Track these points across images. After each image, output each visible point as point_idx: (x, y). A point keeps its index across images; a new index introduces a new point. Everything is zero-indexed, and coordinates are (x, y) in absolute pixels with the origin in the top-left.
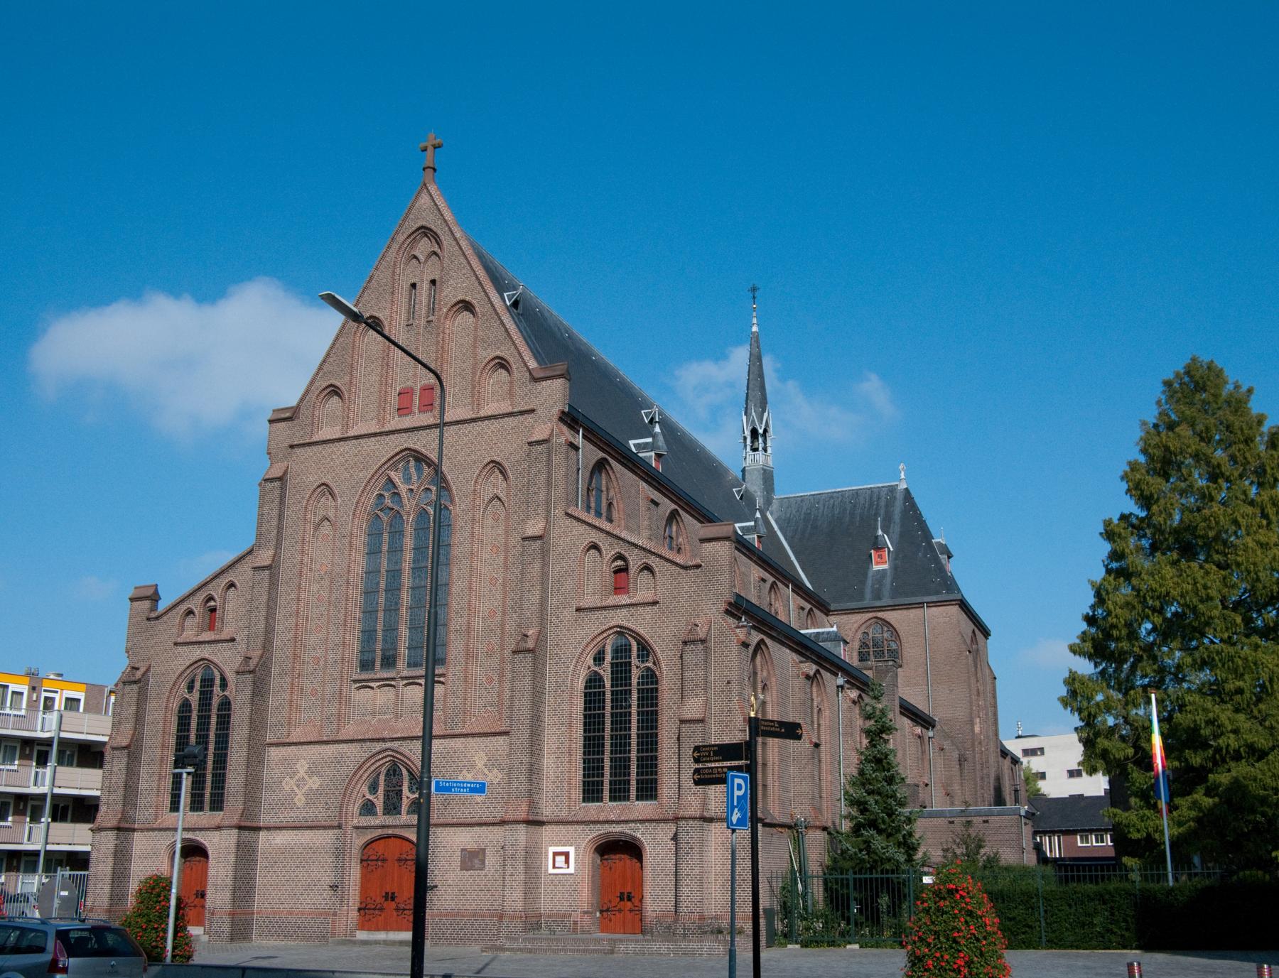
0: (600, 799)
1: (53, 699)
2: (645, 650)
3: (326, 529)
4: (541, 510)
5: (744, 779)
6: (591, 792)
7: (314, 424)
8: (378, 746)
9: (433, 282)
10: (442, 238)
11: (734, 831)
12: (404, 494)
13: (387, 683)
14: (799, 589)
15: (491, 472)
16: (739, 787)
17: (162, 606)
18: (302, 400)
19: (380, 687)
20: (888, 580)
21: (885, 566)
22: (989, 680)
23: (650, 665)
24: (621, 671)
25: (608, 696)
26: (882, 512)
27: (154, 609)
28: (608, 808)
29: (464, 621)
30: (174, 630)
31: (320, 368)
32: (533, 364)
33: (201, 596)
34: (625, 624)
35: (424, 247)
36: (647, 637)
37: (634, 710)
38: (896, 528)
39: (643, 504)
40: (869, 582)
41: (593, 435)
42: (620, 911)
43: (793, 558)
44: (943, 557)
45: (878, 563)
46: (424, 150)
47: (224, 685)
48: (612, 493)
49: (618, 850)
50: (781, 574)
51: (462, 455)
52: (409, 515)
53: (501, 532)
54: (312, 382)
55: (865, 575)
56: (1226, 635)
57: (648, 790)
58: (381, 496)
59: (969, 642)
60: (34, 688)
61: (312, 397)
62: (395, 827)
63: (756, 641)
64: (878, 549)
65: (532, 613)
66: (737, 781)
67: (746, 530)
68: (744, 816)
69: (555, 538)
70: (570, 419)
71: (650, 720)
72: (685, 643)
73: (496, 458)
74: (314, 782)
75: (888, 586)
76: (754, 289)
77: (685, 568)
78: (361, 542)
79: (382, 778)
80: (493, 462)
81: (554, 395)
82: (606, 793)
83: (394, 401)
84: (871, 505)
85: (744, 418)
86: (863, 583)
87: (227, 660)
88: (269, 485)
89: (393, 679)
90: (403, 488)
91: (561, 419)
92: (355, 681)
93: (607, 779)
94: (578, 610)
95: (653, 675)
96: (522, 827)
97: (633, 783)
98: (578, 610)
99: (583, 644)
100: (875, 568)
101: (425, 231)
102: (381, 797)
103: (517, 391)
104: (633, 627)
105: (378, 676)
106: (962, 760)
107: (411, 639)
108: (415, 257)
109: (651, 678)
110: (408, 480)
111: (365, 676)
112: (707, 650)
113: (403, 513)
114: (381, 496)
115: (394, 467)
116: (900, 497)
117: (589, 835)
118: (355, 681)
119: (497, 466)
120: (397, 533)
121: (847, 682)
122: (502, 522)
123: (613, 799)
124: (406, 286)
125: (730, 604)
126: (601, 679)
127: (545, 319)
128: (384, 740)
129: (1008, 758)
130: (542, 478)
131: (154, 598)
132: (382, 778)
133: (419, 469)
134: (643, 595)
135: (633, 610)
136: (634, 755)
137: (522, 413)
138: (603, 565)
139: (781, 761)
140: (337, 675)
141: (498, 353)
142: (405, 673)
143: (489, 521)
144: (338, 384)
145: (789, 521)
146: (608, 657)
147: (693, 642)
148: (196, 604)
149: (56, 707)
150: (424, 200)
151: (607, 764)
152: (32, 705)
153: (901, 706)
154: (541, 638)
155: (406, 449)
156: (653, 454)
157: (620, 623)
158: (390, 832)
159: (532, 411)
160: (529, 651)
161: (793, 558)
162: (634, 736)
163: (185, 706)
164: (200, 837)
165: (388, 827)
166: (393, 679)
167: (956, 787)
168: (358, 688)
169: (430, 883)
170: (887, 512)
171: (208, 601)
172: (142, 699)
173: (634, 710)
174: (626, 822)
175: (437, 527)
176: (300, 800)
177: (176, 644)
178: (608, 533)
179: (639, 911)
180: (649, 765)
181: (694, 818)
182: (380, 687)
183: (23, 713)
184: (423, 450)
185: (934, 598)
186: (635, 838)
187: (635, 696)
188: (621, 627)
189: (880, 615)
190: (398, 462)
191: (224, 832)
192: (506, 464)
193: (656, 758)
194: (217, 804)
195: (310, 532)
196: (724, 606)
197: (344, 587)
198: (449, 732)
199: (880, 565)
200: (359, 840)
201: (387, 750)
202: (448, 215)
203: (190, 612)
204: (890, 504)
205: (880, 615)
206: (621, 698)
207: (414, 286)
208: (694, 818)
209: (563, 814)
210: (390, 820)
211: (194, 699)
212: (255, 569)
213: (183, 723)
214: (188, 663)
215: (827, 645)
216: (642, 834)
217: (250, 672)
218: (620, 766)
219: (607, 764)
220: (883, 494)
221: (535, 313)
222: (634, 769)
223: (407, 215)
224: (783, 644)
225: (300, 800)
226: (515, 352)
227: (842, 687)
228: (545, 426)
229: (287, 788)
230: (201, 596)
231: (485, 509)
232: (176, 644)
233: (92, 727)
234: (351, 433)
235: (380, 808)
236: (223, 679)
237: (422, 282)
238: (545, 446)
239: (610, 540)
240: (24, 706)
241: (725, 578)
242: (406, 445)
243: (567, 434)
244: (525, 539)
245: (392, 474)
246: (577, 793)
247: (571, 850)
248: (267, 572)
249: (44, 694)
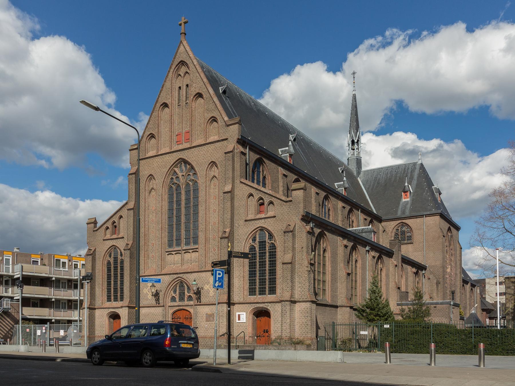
0: (255, 295)
1: (77, 265)
2: (271, 236)
3: (153, 193)
4: (230, 181)
6: (252, 292)
7: (146, 151)
8: (176, 276)
9: (187, 85)
10: (189, 65)
11: (217, 289)
12: (181, 177)
13: (178, 252)
15: (212, 166)
16: (219, 274)
17: (98, 225)
19: (176, 254)
20: (409, 206)
21: (408, 199)
22: (458, 249)
23: (273, 242)
24: (262, 244)
25: (258, 255)
26: (409, 175)
27: (95, 227)
28: (258, 298)
29: (204, 226)
30: (103, 235)
32: (226, 119)
33: (111, 221)
34: (264, 226)
35: (183, 69)
36: (271, 231)
37: (267, 260)
38: (415, 182)
39: (280, 176)
40: (400, 207)
41: (254, 148)
42: (264, 336)
43: (368, 197)
44: (437, 195)
45: (405, 198)
46: (180, 25)
47: (121, 255)
48: (265, 173)
49: (262, 314)
51: (198, 158)
52: (183, 184)
53: (217, 190)
55: (399, 204)
57: (273, 291)
58: (172, 178)
59: (445, 232)
60: (70, 261)
61: (144, 139)
62: (183, 306)
64: (405, 192)
65: (228, 223)
67: (339, 186)
69: (237, 192)
70: (242, 142)
71: (273, 263)
72: (285, 232)
73: (213, 160)
75: (408, 209)
76: (354, 73)
77: (286, 202)
78: (166, 197)
79: (178, 288)
80: (212, 162)
81: (234, 132)
82: (257, 292)
83: (175, 138)
84: (404, 172)
85: (349, 135)
86: (398, 207)
87: (121, 244)
88: (131, 176)
89: (180, 251)
90: (180, 174)
91: (238, 142)
92: (167, 252)
93: (257, 287)
94: (246, 221)
97: (267, 288)
98: (246, 221)
99: (248, 234)
100: (404, 200)
101: (183, 63)
102: (178, 295)
103: (221, 131)
104: (266, 227)
105: (175, 250)
106: (438, 283)
107: (186, 235)
108: (180, 75)
109: (273, 247)
110: (182, 171)
111: (170, 250)
112: (294, 236)
113: (180, 184)
114: (172, 178)
115: (176, 166)
117: (251, 307)
118: (167, 252)
119: (213, 164)
120: (179, 194)
122: (217, 187)
124: (177, 89)
125: (303, 216)
126: (255, 248)
127: (242, 97)
128: (177, 274)
129: (469, 284)
130: (230, 167)
131: (95, 223)
132: (178, 288)
133: (186, 167)
135: (266, 220)
136: (267, 277)
137: (223, 140)
138: (253, 202)
139: (332, 280)
140: (160, 250)
141: (213, 115)
142: (184, 248)
143: (212, 186)
144: (153, 133)
146: (258, 240)
147: (288, 232)
148: (109, 224)
149: (79, 267)
150: (182, 47)
151: (258, 281)
152: (70, 267)
153: (402, 258)
154: (232, 232)
155: (180, 159)
156: (288, 154)
157: (261, 225)
158: (181, 308)
159: (227, 139)
160: (226, 238)
161: (368, 197)
162: (267, 270)
163: (109, 263)
164: (117, 311)
165: (180, 306)
166: (180, 251)
167: (435, 294)
168: (168, 255)
170: (411, 175)
171: (113, 224)
172: (94, 260)
173: (267, 260)
174: (264, 303)
175: (193, 190)
177: (104, 240)
178: (256, 189)
179: (269, 336)
180: (273, 281)
181: (287, 301)
182: (176, 254)
183: (67, 269)
184: (186, 159)
185: (429, 213)
186: (267, 309)
187: (267, 254)
188: (262, 227)
189: (404, 221)
190: (178, 164)
191: (124, 308)
192: (217, 162)
194: (122, 299)
195: (147, 194)
196: (301, 217)
197: (160, 216)
198: (200, 270)
199: (406, 199)
200: (171, 311)
201: (178, 277)
202: (191, 55)
203: (107, 228)
204: (413, 171)
205: (404, 221)
206: (262, 255)
207: (180, 88)
208: (287, 301)
209: (242, 300)
210: (181, 303)
211: (112, 260)
212: (128, 210)
213: (109, 270)
214: (108, 247)
215: (364, 235)
216: (270, 307)
217: (129, 249)
218: (262, 282)
219: (258, 281)
220: (410, 167)
221: (236, 95)
222: (267, 283)
223: (175, 56)
226: (219, 114)
227: (368, 251)
228: (231, 145)
229: (145, 292)
230: (111, 221)
231: (210, 182)
232: (104, 240)
234: (159, 153)
235: (177, 300)
236: (121, 253)
237: (183, 86)
238: (231, 153)
239: (257, 192)
240: (67, 267)
241: (302, 205)
242: (180, 157)
243: (241, 149)
244: (224, 193)
245: (176, 169)
246: (247, 292)
248: (132, 211)
249: (74, 263)
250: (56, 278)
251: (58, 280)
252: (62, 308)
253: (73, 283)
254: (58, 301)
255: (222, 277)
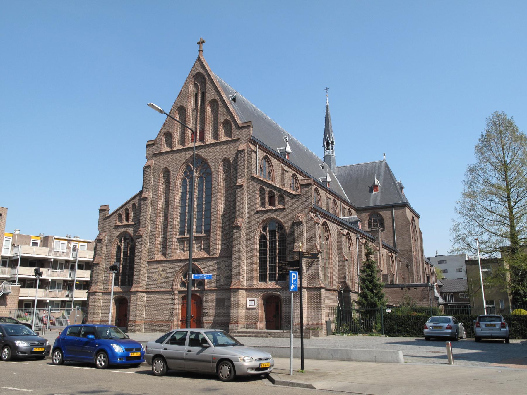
5: (296, 273)
6: (263, 278)
14: (344, 201)
16: (294, 276)
18: (157, 137)
20: (379, 198)
26: (377, 172)
31: (163, 126)
38: (382, 178)
41: (262, 147)
50: (336, 196)
54: (161, 131)
56: (473, 213)
63: (323, 222)
66: (293, 274)
68: (296, 287)
74: (164, 275)
76: (327, 89)
84: (372, 169)
95: (284, 235)
96: (244, 291)
116: (383, 165)
121: (360, 236)
123: (39, 288)
127: (246, 105)
134: (279, 206)
145: (341, 176)
169: (204, 310)
170: (378, 172)
176: (159, 281)
183: (65, 251)
189: (414, 216)
193: (56, 268)
204: (379, 169)
224: (334, 223)
225: (159, 281)
233: (87, 255)
247: (256, 299)
250: (54, 259)
251: (56, 261)
252: (58, 289)
253: (70, 264)
254: (54, 281)
255: (296, 280)
